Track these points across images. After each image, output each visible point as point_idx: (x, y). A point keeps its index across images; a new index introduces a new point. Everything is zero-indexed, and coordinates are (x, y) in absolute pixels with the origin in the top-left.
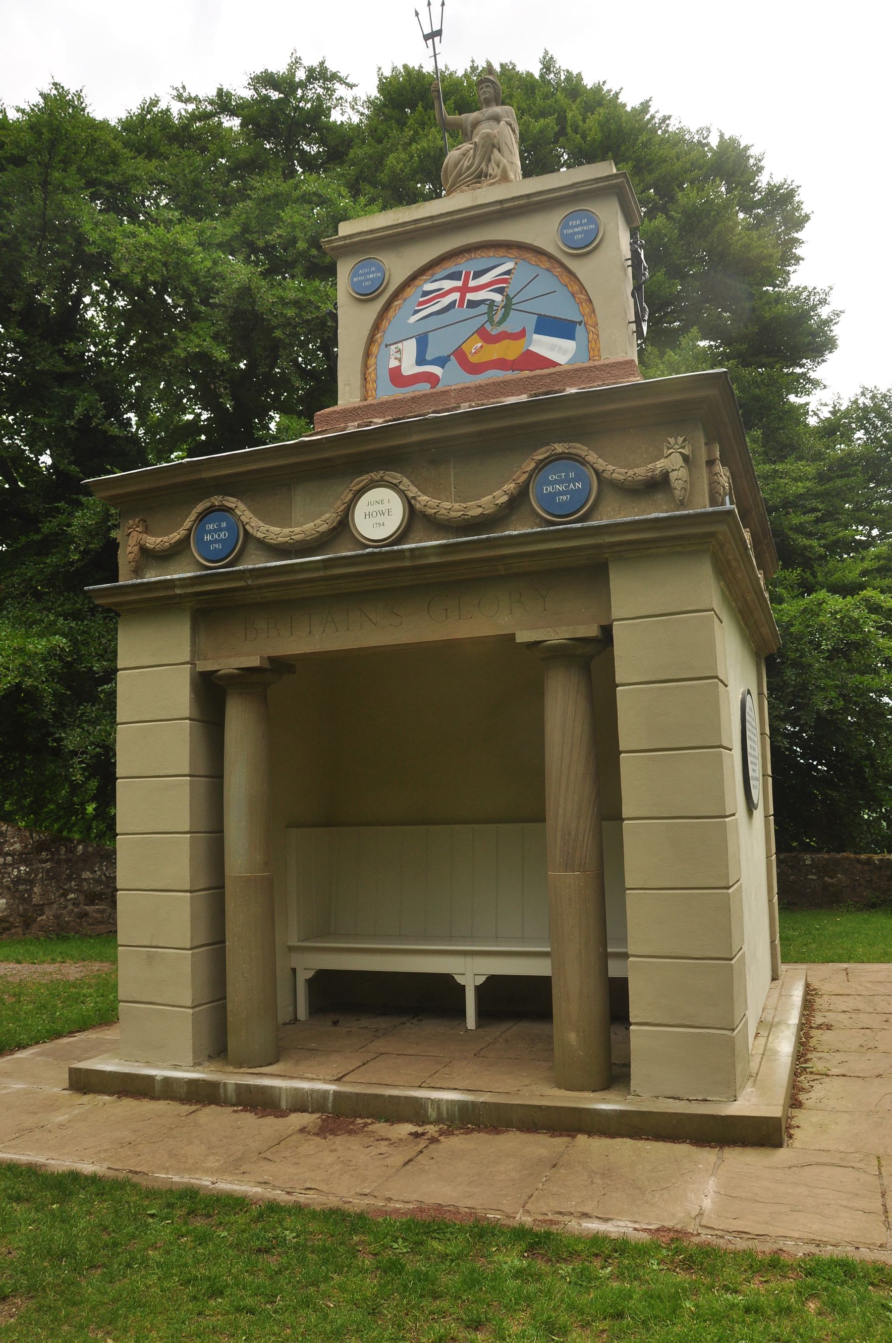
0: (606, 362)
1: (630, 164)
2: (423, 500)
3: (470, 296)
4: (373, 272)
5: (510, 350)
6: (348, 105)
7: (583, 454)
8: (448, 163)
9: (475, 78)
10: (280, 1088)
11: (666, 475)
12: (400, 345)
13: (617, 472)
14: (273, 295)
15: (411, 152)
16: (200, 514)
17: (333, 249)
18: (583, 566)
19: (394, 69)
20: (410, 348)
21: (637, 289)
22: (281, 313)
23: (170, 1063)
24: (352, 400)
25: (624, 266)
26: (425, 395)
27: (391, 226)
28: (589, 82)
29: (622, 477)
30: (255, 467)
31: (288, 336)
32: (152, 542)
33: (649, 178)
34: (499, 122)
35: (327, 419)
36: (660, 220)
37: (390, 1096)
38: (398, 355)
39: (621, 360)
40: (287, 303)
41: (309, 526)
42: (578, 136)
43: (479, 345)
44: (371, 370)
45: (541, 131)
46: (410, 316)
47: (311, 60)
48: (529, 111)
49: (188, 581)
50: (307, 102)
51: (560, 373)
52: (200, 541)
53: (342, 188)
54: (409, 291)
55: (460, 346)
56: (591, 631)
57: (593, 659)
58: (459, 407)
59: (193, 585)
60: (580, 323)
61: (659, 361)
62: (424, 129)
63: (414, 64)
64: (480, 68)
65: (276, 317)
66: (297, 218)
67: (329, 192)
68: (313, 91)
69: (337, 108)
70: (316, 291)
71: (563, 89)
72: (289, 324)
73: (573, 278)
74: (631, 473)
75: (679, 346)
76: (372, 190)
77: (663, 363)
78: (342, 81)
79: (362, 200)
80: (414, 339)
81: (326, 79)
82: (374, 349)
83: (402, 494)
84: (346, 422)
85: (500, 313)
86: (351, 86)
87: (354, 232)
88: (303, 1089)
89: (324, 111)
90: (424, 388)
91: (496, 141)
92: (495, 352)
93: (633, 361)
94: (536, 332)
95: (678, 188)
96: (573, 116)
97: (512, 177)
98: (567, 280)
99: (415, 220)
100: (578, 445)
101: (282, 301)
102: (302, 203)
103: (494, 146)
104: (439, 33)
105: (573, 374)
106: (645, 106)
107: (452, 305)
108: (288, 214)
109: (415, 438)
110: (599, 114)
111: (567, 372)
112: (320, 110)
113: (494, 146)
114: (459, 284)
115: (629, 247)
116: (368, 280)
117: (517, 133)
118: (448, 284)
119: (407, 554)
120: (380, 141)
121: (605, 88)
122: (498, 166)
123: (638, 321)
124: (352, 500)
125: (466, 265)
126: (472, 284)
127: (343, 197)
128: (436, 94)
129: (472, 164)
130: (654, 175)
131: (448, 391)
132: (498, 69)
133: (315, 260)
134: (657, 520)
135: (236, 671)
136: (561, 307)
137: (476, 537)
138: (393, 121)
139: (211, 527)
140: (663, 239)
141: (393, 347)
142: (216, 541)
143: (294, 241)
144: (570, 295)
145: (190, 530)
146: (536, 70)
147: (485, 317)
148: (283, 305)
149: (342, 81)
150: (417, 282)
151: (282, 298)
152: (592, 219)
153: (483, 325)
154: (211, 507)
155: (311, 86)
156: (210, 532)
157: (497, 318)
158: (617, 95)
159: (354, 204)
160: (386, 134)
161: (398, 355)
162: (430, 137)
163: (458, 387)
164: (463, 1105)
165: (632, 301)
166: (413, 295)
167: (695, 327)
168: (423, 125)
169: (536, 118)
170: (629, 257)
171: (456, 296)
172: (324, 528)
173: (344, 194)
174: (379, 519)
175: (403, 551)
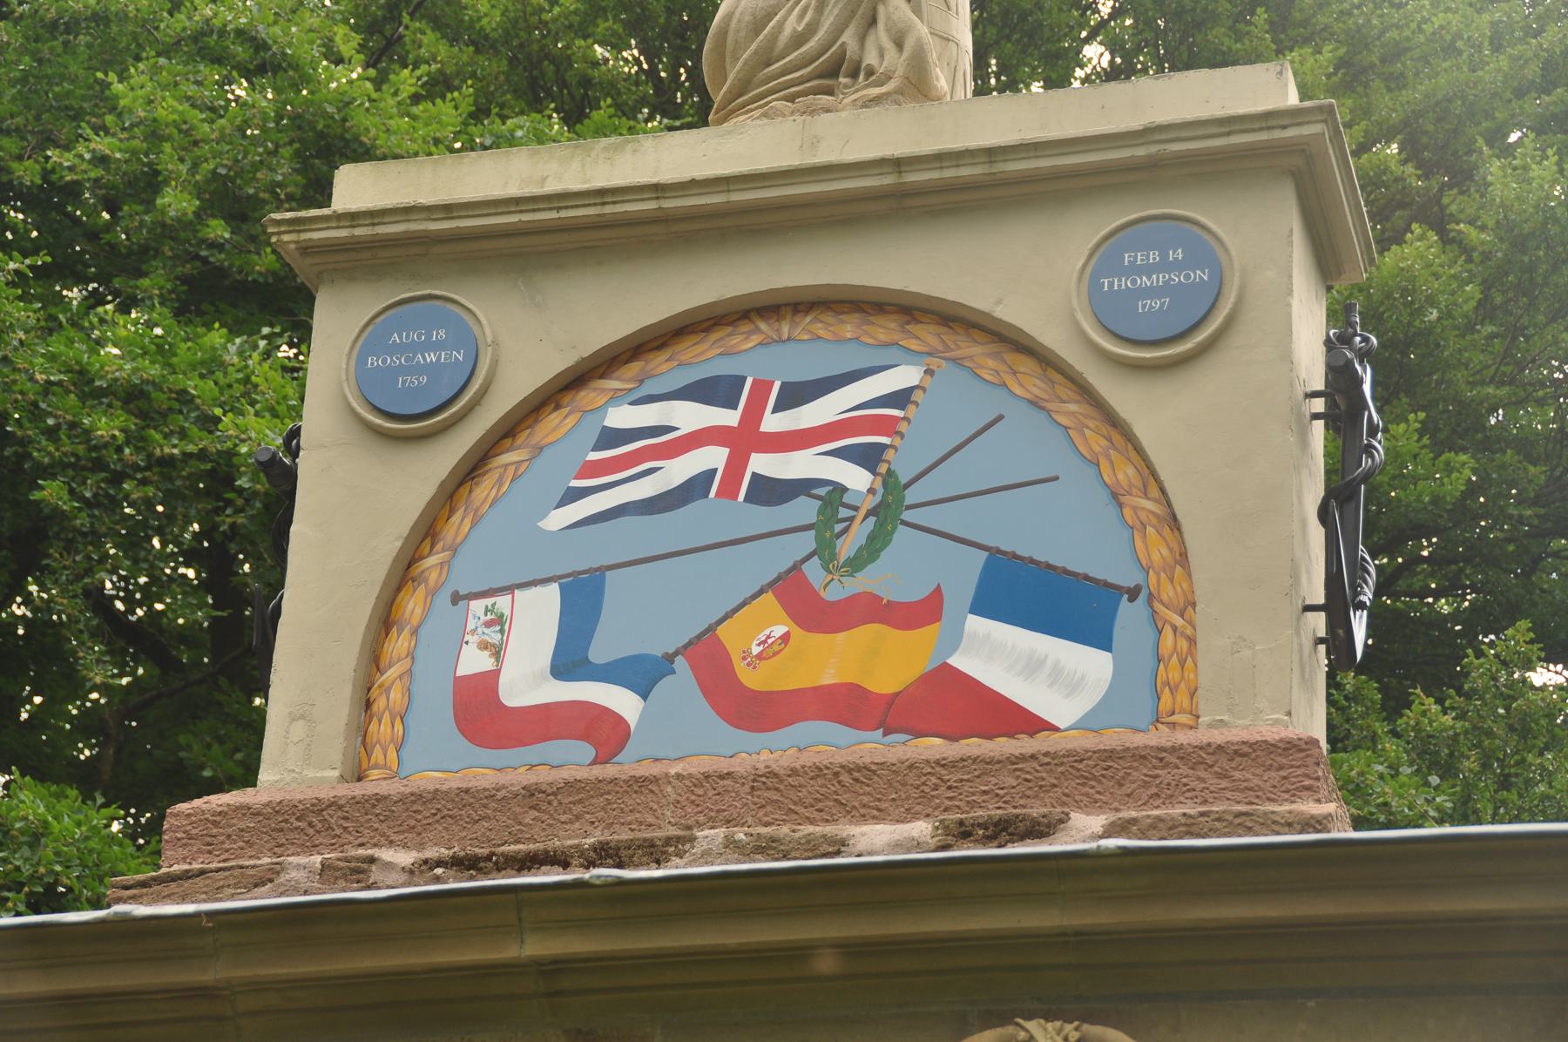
0: (1218, 737)
1: (1328, 53)
3: (761, 464)
4: (437, 347)
5: (886, 661)
12: (503, 602)
14: (52, 358)
17: (306, 249)
20: (537, 616)
21: (1338, 498)
22: (73, 425)
24: (311, 773)
25: (1300, 415)
26: (572, 786)
27: (517, 201)
33: (1389, 106)
35: (210, 833)
36: (1418, 250)
38: (493, 636)
39: (1271, 734)
40: (100, 393)
43: (779, 630)
44: (392, 673)
46: (547, 506)
51: (1051, 760)
53: (341, 31)
54: (554, 424)
55: (711, 629)
58: (678, 844)
60: (1133, 593)
61: (1381, 728)
65: (52, 433)
66: (169, 108)
70: (211, 366)
72: (99, 465)
73: (1116, 437)
75: (1457, 681)
76: (443, 50)
77: (1395, 734)
79: (407, 80)
80: (554, 588)
82: (412, 605)
84: (278, 848)
85: (860, 532)
90: (570, 758)
92: (831, 659)
93: (1315, 742)
94: (979, 608)
95: (1490, 143)
98: (1098, 444)
99: (602, 192)
101: (85, 385)
102: (190, 60)
105: (1094, 771)
107: (696, 487)
108: (134, 90)
109: (535, 947)
111: (1076, 757)
114: (729, 418)
115: (1321, 350)
116: (401, 349)
118: (690, 416)
122: (899, 45)
123: (1337, 606)
125: (755, 357)
126: (772, 422)
127: (339, 61)
129: (811, 29)
130: (1406, 95)
131: (655, 780)
133: (217, 258)
136: (1072, 531)
140: (1420, 311)
141: (477, 606)
143: (150, 183)
144: (1104, 495)
147: (808, 541)
148: (83, 397)
150: (587, 397)
151: (82, 372)
152: (1205, 250)
153: (796, 567)
157: (847, 547)
159: (378, 89)
161: (493, 636)
163: (694, 767)
165: (1317, 534)
166: (566, 436)
167: (1524, 624)
170: (1319, 385)
171: (714, 457)
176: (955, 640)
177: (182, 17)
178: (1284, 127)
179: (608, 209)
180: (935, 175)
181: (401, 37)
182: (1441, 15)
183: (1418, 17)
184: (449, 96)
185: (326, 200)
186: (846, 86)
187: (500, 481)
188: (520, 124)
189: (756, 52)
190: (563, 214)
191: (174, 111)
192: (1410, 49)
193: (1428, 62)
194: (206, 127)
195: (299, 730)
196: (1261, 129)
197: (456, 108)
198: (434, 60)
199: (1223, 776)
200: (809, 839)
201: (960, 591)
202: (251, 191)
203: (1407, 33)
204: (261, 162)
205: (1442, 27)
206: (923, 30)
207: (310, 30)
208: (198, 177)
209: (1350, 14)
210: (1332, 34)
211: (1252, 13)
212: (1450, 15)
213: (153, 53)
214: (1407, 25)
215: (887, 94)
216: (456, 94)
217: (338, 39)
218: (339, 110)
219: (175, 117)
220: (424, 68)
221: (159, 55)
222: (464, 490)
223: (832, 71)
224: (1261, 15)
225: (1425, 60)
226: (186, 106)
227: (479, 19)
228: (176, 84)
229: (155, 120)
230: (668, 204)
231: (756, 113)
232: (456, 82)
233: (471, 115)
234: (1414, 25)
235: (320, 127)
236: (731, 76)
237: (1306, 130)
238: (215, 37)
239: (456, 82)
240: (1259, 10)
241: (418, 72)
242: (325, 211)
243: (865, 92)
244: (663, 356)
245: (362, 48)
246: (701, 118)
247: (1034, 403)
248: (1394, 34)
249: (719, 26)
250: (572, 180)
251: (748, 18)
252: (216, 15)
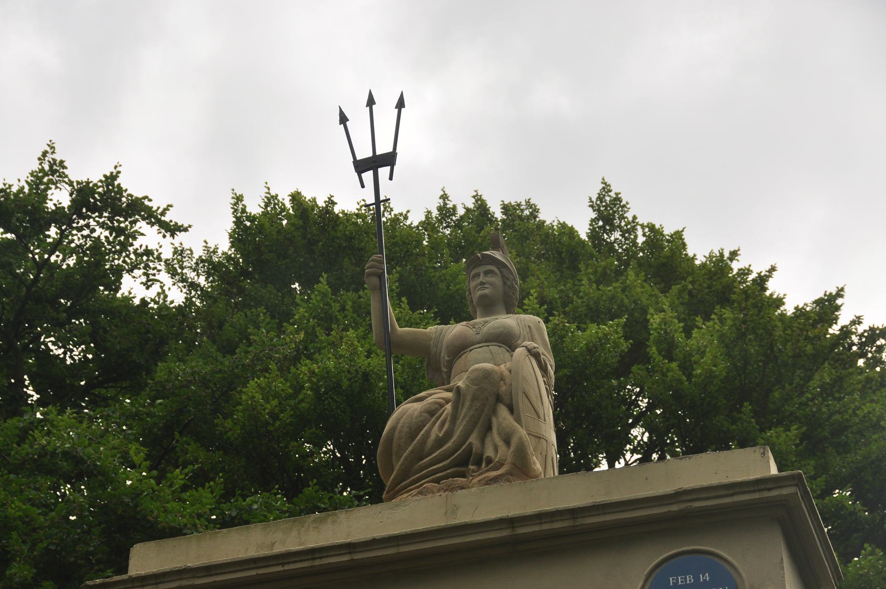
1: (794, 430)
6: (162, 266)
8: (393, 429)
9: (448, 232)
15: (296, 377)
19: (271, 200)
28: (699, 250)
34: (512, 348)
42: (674, 365)
45: (591, 349)
47: (87, 169)
48: (564, 305)
50: (68, 252)
53: (133, 447)
62: (328, 331)
63: (316, 193)
64: (461, 212)
67: (102, 454)
68: (86, 232)
69: (137, 272)
71: (640, 263)
76: (202, 455)
78: (153, 217)
79: (178, 476)
81: (117, 211)
86: (173, 229)
87: (167, 567)
89: (105, 274)
91: (504, 388)
96: (664, 322)
97: (538, 467)
99: (313, 551)
103: (499, 399)
104: (389, 159)
106: (828, 307)
110: (722, 321)
112: (98, 271)
113: (499, 399)
117: (551, 372)
120: (229, 349)
121: (736, 266)
122: (507, 442)
128: (375, 280)
129: (449, 435)
132: (499, 215)
138: (262, 309)
149: (153, 217)
155: (82, 222)
158: (761, 281)
159: (158, 484)
160: (245, 336)
162: (343, 349)
168: (327, 320)
169: (581, 321)
173: (136, 459)
177: (27, 446)
178: (770, 490)
179: (317, 562)
180: (536, 528)
181: (174, 448)
182: (868, 404)
183: (853, 406)
184: (207, 484)
185: (124, 569)
186: (474, 471)
188: (255, 502)
189: (412, 452)
190: (287, 567)
191: (20, 509)
192: (849, 427)
193: (863, 436)
194: (42, 518)
196: (754, 491)
197: (212, 492)
198: (197, 462)
202: (72, 559)
203: (846, 416)
204: (79, 539)
205: (869, 412)
206: (523, 432)
207: (114, 448)
208: (35, 553)
209: (807, 405)
210: (796, 418)
211: (742, 406)
212: (874, 405)
213: (6, 472)
214: (847, 412)
215: (501, 476)
216: (212, 483)
217: (132, 453)
218: (132, 499)
219: (21, 513)
220: (190, 467)
221: (10, 473)
223: (464, 461)
224: (747, 407)
225: (860, 433)
226: (27, 506)
227: (226, 432)
228: (22, 491)
229: (6, 517)
230: (357, 556)
231: (414, 492)
232: (212, 475)
233: (222, 496)
234: (850, 411)
235: (119, 512)
236: (397, 468)
237: (785, 491)
238: (48, 457)
239: (212, 475)
240: (746, 404)
241: (186, 471)
242: (124, 577)
243: (486, 475)
245: (148, 457)
246: (376, 498)
248: (837, 417)
249: (389, 432)
250: (293, 546)
251: (406, 430)
252: (49, 443)
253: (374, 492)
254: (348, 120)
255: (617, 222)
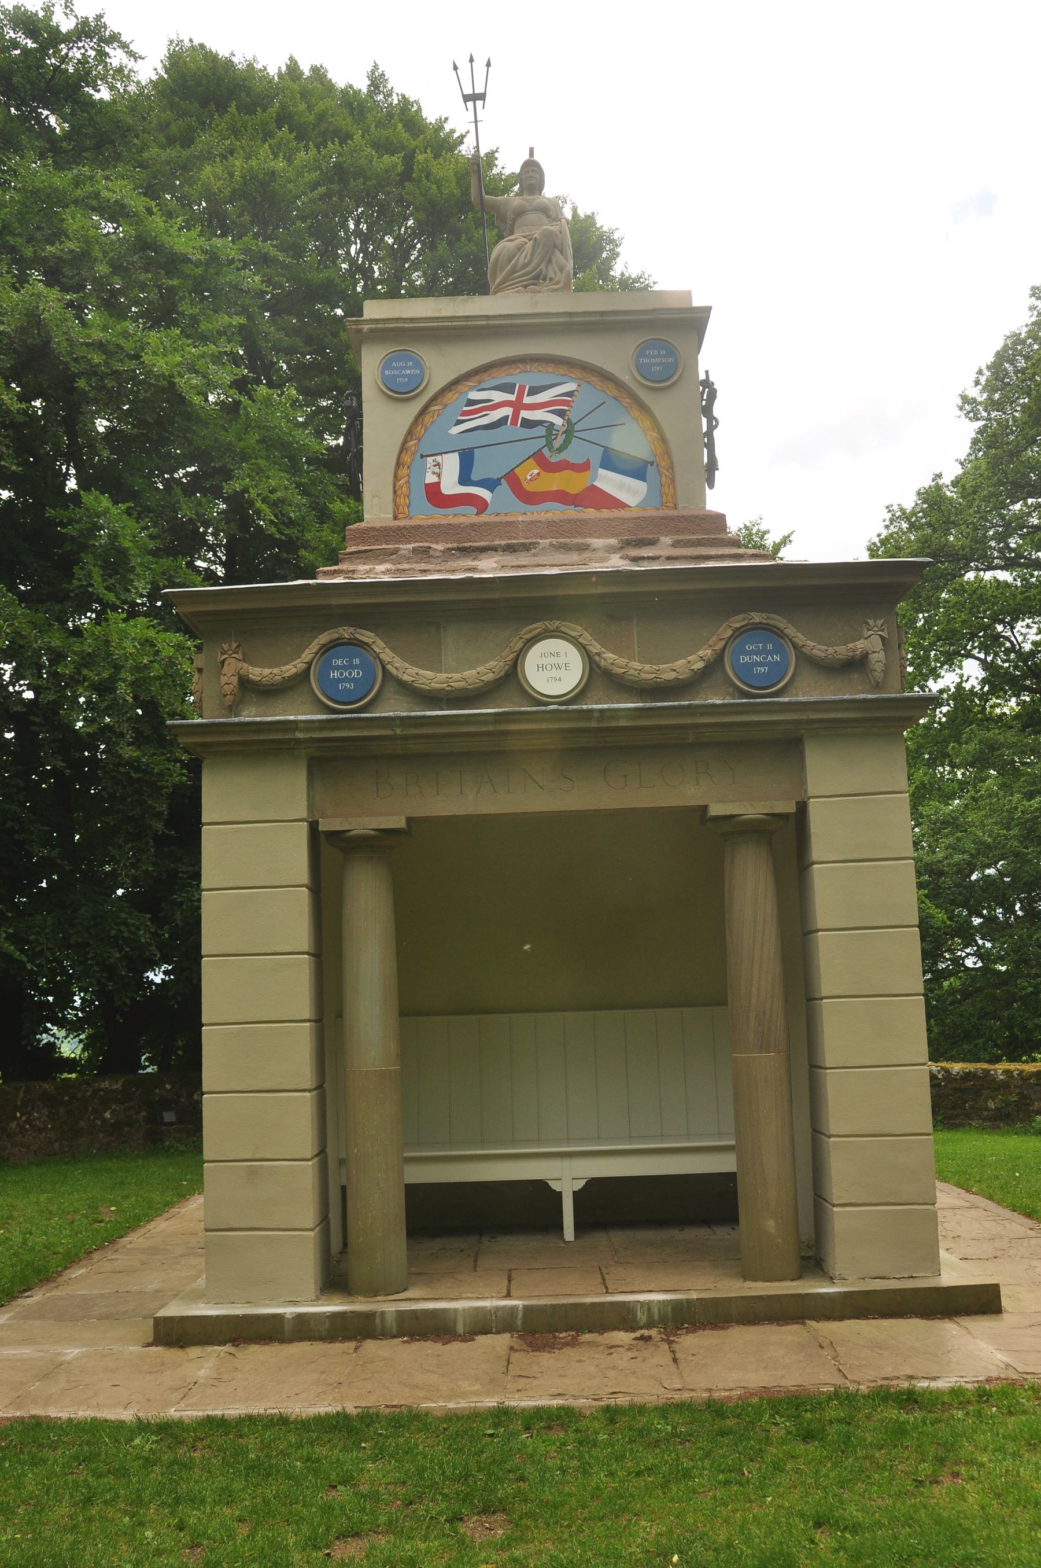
0: (685, 513)
2: (609, 658)
3: (524, 414)
4: (410, 368)
7: (782, 626)
8: (499, 256)
10: (456, 1310)
11: (865, 656)
12: (439, 458)
13: (818, 649)
16: (324, 645)
18: (783, 744)
20: (451, 464)
23: (282, 1299)
29: (823, 654)
30: (402, 599)
31: (94, 388)
32: (257, 673)
37: (592, 1304)
41: (470, 673)
43: (536, 471)
49: (317, 724)
52: (323, 678)
54: (450, 396)
56: (790, 808)
57: (787, 840)
59: (320, 729)
60: (652, 464)
65: (75, 360)
72: (95, 374)
74: (831, 650)
78: (124, 46)
81: (101, 40)
83: (582, 648)
86: (132, 55)
88: (486, 1307)
90: (467, 515)
92: (554, 482)
100: (776, 616)
104: (482, 97)
107: (503, 421)
112: (85, 75)
113: (555, 246)
116: (396, 368)
118: (498, 396)
119: (596, 714)
122: (561, 270)
124: (521, 650)
126: (527, 400)
129: (530, 262)
134: (865, 701)
135: (372, 833)
137: (676, 703)
139: (339, 662)
141: (430, 459)
142: (346, 680)
145: (310, 664)
146: (362, 85)
147: (543, 442)
149: (124, 46)
150: (461, 387)
153: (540, 450)
154: (338, 639)
156: (338, 668)
157: (557, 444)
164: (677, 1305)
166: (455, 402)
171: (508, 411)
172: (490, 677)
174: (555, 673)
175: (592, 711)
176: (595, 477)
179: (469, 323)
180: (582, 319)
187: (433, 416)
195: (376, 501)
199: (698, 525)
200: (578, 544)
201: (595, 461)
222: (420, 419)
223: (537, 277)
244: (487, 374)
247: (615, 398)
253: (482, 289)
254: (574, 1192)
255: (381, 89)
